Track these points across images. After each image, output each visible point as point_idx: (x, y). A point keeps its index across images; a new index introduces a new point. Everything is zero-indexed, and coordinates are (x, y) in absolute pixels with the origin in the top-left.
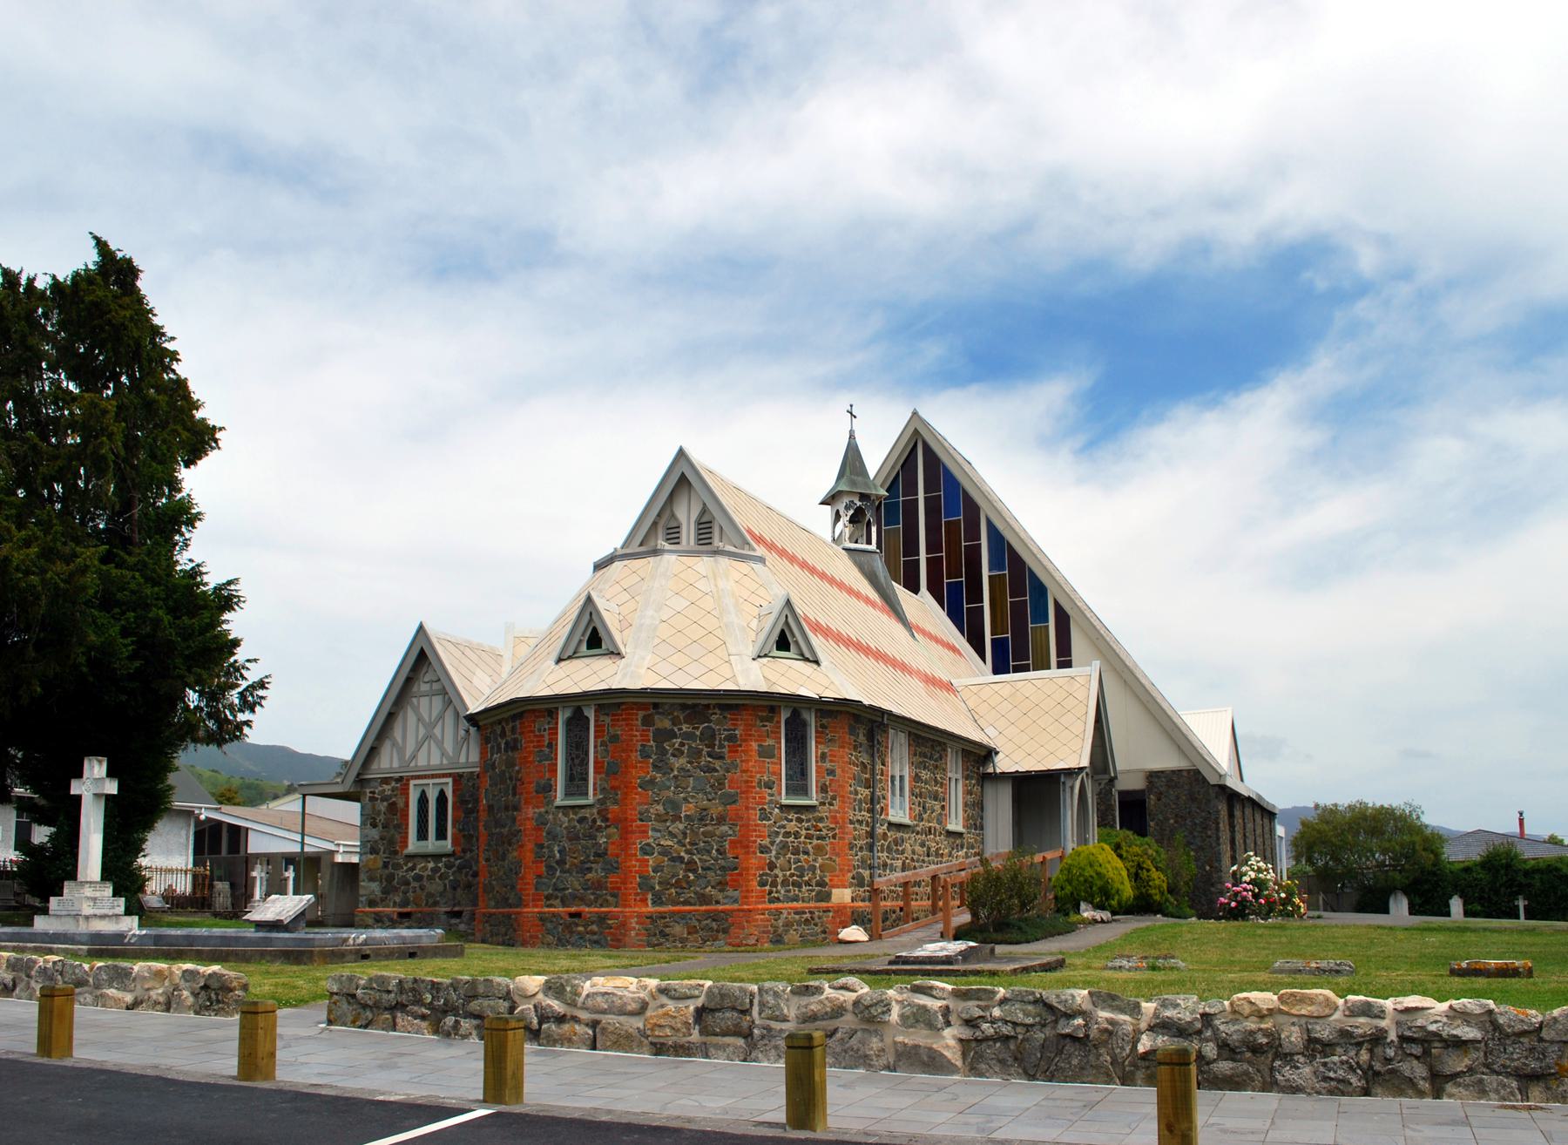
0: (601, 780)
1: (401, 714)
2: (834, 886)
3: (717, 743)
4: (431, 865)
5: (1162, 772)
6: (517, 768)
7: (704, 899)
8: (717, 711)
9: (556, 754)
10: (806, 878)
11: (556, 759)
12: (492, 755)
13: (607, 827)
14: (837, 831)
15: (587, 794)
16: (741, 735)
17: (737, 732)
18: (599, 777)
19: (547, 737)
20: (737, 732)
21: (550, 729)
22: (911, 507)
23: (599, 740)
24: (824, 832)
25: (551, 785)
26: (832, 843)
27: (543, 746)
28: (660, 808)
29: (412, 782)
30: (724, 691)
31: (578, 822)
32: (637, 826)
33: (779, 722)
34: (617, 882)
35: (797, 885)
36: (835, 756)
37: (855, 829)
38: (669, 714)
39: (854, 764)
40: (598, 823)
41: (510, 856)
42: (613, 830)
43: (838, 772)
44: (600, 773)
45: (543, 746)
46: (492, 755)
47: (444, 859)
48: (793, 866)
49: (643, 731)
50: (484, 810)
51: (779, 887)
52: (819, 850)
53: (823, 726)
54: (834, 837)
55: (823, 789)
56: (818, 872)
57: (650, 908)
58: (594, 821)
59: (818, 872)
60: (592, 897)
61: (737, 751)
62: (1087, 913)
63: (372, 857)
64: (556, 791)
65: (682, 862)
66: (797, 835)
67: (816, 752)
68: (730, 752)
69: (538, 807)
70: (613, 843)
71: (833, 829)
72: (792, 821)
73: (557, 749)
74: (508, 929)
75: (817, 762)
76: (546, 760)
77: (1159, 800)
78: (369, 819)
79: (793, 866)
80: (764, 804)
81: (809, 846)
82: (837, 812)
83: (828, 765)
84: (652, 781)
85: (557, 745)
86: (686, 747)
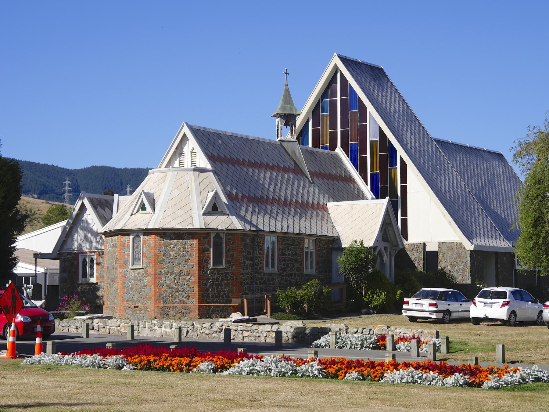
0: (145, 259)
1: (75, 227)
2: (233, 298)
3: (186, 246)
4: (88, 287)
5: (445, 243)
6: (116, 254)
7: (181, 302)
8: (186, 235)
9: (130, 250)
10: (221, 295)
11: (130, 252)
12: (108, 248)
13: (147, 276)
14: (234, 277)
15: (140, 264)
16: (195, 244)
17: (194, 243)
18: (144, 258)
19: (126, 244)
20: (194, 243)
21: (127, 241)
22: (333, 104)
23: (144, 245)
24: (229, 278)
25: (128, 261)
26: (232, 282)
27: (125, 247)
28: (165, 270)
29: (80, 255)
30: (188, 228)
31: (137, 274)
32: (157, 276)
33: (210, 238)
34: (150, 296)
35: (217, 297)
36: (234, 250)
37: (243, 276)
38: (169, 236)
39: (244, 252)
40: (144, 275)
41: (114, 286)
42: (149, 277)
43: (235, 255)
44: (145, 257)
45: (125, 247)
46: (108, 248)
47: (93, 285)
48: (216, 290)
49: (160, 242)
50: (106, 268)
51: (210, 298)
52: (226, 285)
53: (229, 239)
54: (233, 279)
55: (228, 262)
56: (226, 292)
57: (162, 305)
58: (143, 274)
59: (226, 292)
60: (142, 301)
61: (194, 250)
62: (80, 302)
63: (65, 284)
64: (129, 263)
65: (174, 289)
66: (218, 279)
67: (226, 249)
68: (191, 250)
69: (124, 269)
70: (149, 282)
71: (233, 277)
72: (215, 274)
73: (130, 248)
74: (114, 312)
75: (226, 252)
76: (127, 252)
77: (444, 256)
78: (63, 268)
79: (216, 290)
80: (204, 268)
81: (223, 283)
82: (234, 270)
83: (231, 253)
84: (163, 260)
85: (130, 246)
86: (175, 248)
